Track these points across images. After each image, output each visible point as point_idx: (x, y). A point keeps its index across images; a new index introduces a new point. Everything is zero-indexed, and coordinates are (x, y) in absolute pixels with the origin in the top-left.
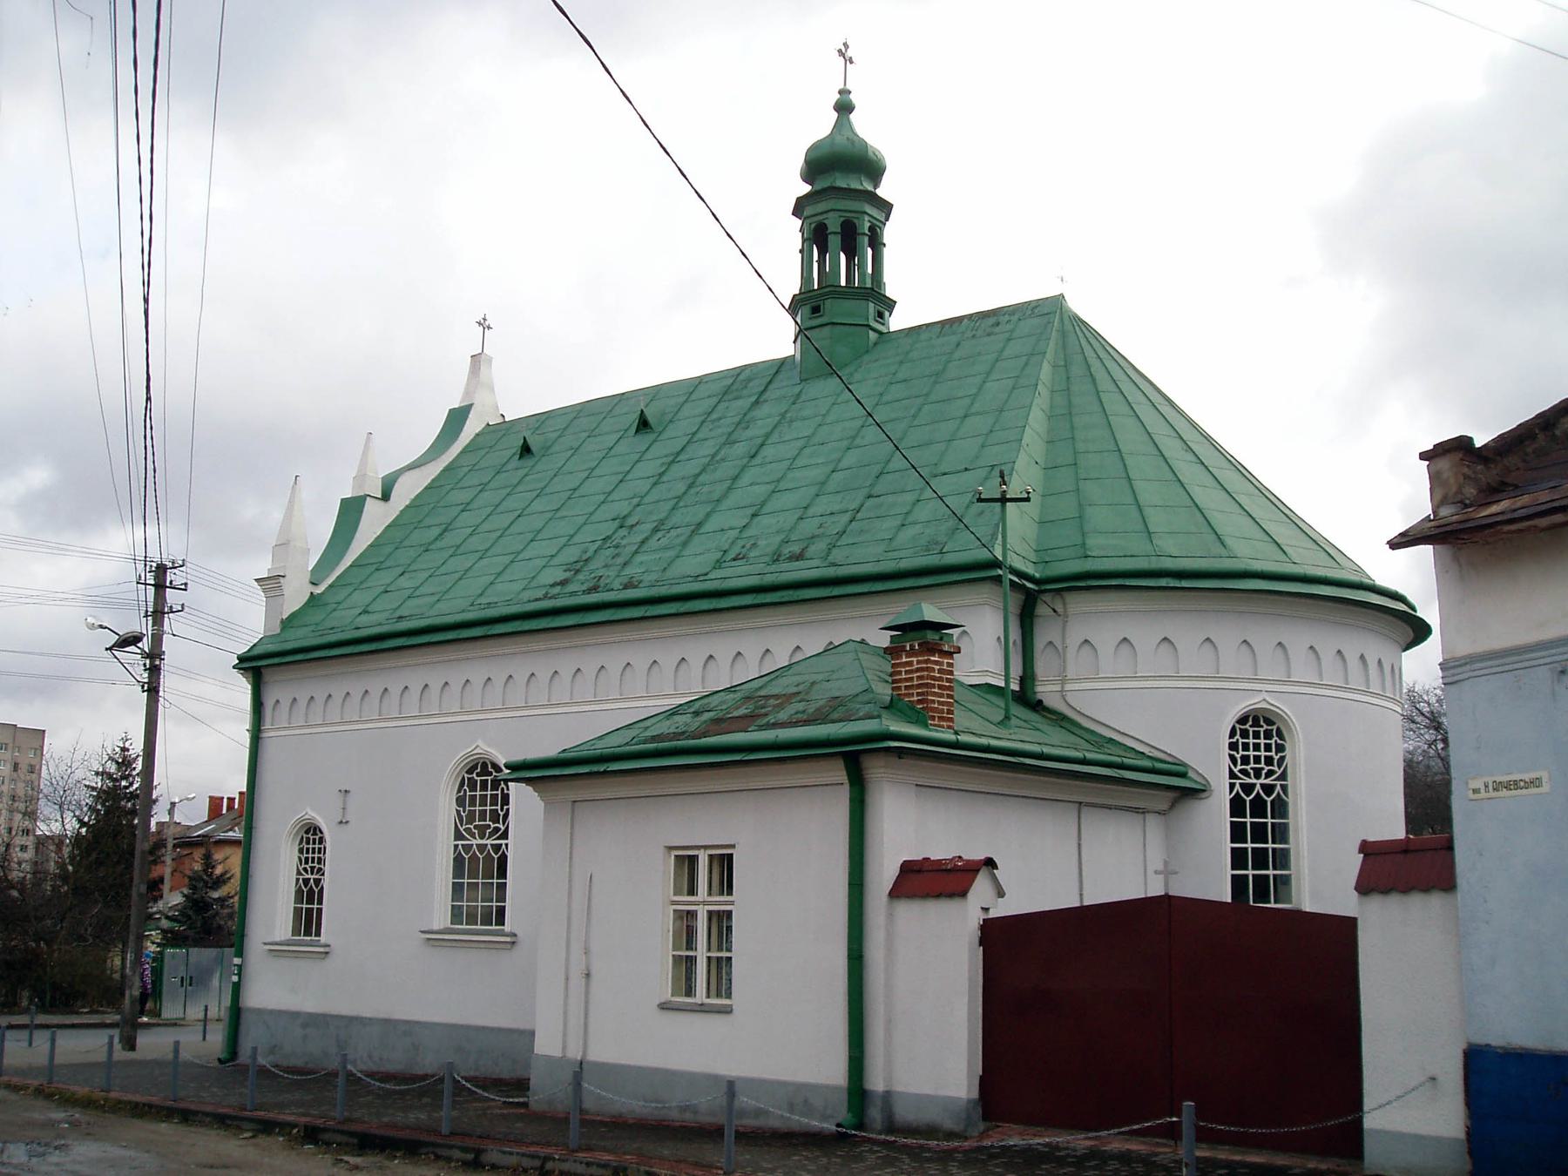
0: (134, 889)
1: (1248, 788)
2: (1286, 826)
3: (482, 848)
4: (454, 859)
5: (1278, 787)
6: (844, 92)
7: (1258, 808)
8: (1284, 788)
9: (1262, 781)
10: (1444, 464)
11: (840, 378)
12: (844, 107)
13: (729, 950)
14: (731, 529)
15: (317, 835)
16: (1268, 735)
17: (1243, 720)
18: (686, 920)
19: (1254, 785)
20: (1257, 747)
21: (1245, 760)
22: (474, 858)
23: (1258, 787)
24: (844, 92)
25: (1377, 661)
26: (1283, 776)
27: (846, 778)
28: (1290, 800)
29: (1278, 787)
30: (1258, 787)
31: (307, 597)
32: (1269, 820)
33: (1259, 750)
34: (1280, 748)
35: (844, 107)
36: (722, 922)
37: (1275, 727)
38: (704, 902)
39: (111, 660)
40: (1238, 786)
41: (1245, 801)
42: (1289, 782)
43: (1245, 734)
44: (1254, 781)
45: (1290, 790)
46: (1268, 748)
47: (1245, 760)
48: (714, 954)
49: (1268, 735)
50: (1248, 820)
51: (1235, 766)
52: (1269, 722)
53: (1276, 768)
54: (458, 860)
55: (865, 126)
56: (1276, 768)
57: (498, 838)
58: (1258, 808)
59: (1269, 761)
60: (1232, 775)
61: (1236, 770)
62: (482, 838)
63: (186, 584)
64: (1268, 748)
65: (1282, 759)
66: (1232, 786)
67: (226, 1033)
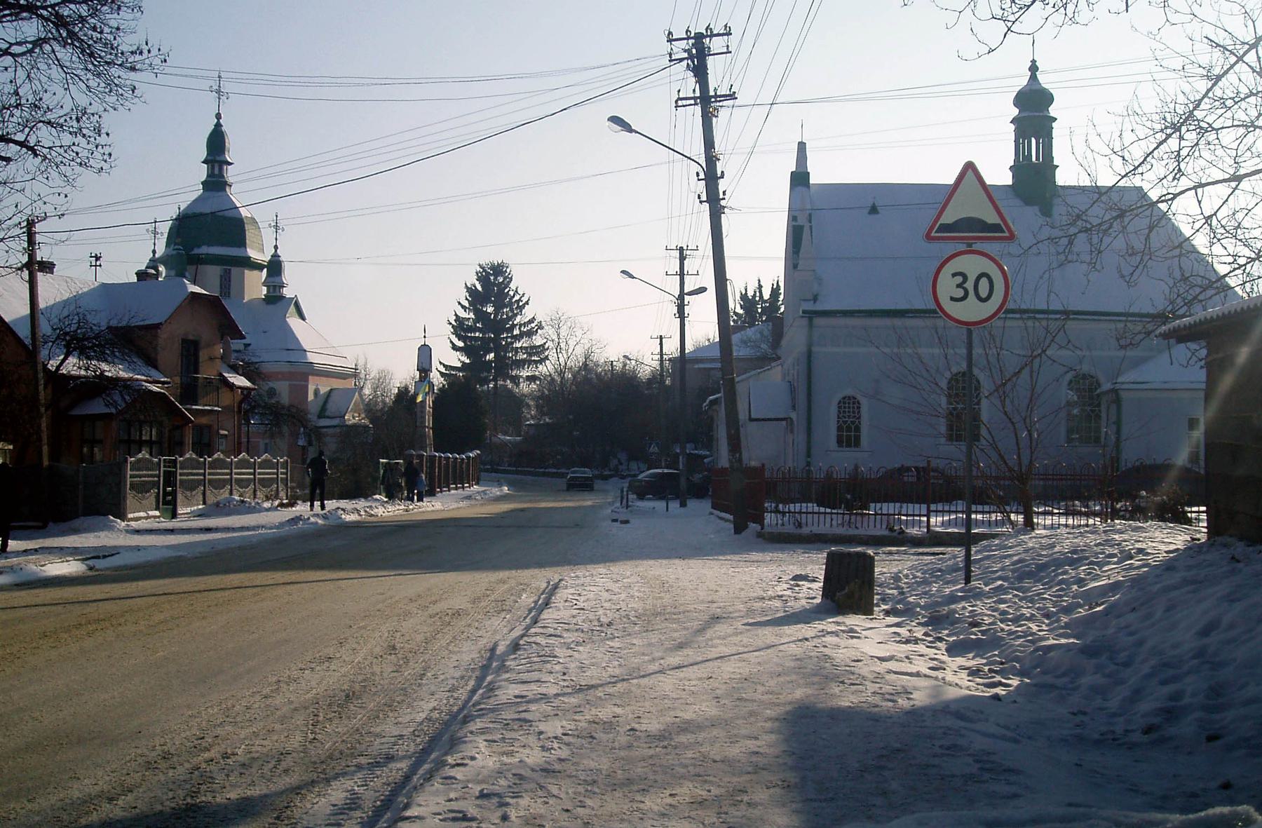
1: (845, 422)
2: (838, 431)
6: (1034, 62)
7: (849, 429)
11: (1223, 128)
12: (1034, 68)
14: (1044, 273)
16: (844, 403)
17: (844, 398)
21: (844, 412)
24: (1034, 62)
25: (271, 307)
26: (859, 418)
27: (823, 572)
31: (303, 345)
35: (1034, 68)
43: (844, 403)
47: (844, 412)
55: (1044, 80)
58: (849, 429)
59: (854, 412)
66: (838, 421)
67: (74, 574)
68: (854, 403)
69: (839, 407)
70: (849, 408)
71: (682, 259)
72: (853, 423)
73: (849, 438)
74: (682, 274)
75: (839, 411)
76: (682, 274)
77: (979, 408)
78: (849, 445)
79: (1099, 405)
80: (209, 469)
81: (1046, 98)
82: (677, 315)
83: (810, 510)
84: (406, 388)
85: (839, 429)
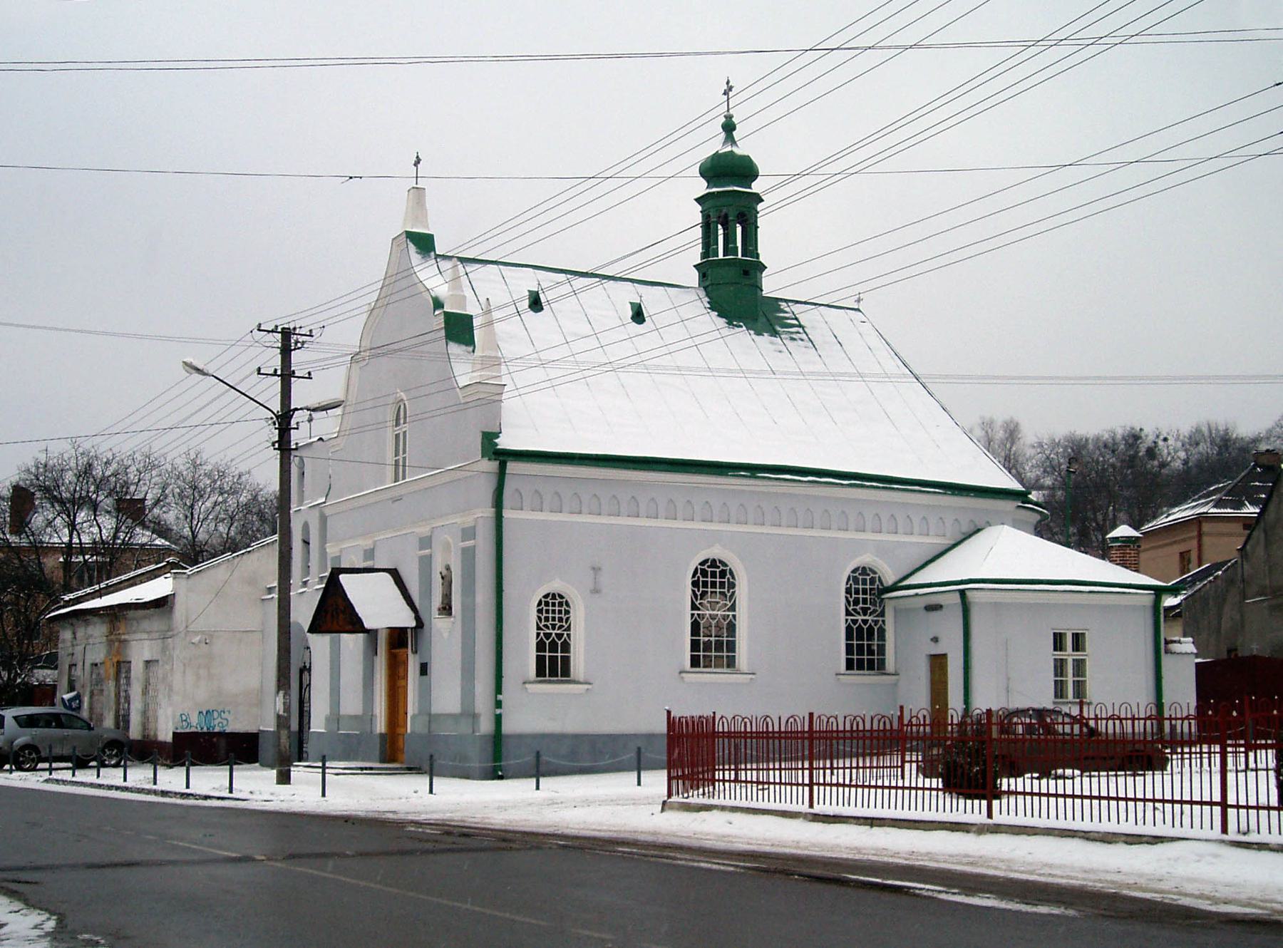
0: (49, 672)
1: (548, 636)
3: (865, 622)
4: (537, 644)
5: (565, 635)
6: (729, 118)
7: (553, 647)
8: (569, 635)
9: (556, 631)
10: (709, 204)
13: (1056, 681)
15: (862, 608)
16: (561, 604)
17: (546, 596)
18: (1060, 667)
19: (551, 634)
20: (554, 612)
21: (547, 619)
22: (860, 629)
23: (554, 635)
24: (729, 118)
26: (569, 629)
28: (572, 643)
29: (565, 635)
30: (554, 635)
32: (547, 654)
33: (866, 594)
34: (567, 612)
36: (1079, 666)
37: (877, 576)
38: (1069, 655)
39: (909, 380)
40: (542, 635)
41: (545, 643)
42: (572, 632)
43: (547, 604)
44: (551, 631)
45: (886, 623)
46: (547, 611)
48: (1076, 679)
49: (561, 604)
50: (547, 654)
51: (850, 606)
52: (561, 597)
53: (564, 624)
54: (849, 630)
56: (564, 624)
57: (877, 616)
58: (553, 647)
59: (561, 620)
60: (539, 628)
61: (541, 625)
62: (865, 615)
63: (309, 373)
64: (560, 612)
65: (568, 619)
66: (538, 635)
68: (547, 604)
69: (540, 611)
70: (554, 612)
71: (286, 351)
72: (559, 636)
73: (553, 660)
74: (286, 375)
75: (539, 618)
76: (286, 375)
77: (734, 616)
78: (553, 673)
79: (882, 614)
80: (545, 676)
81: (742, 170)
82: (277, 445)
83: (934, 786)
84: (1085, 446)
85: (540, 646)
